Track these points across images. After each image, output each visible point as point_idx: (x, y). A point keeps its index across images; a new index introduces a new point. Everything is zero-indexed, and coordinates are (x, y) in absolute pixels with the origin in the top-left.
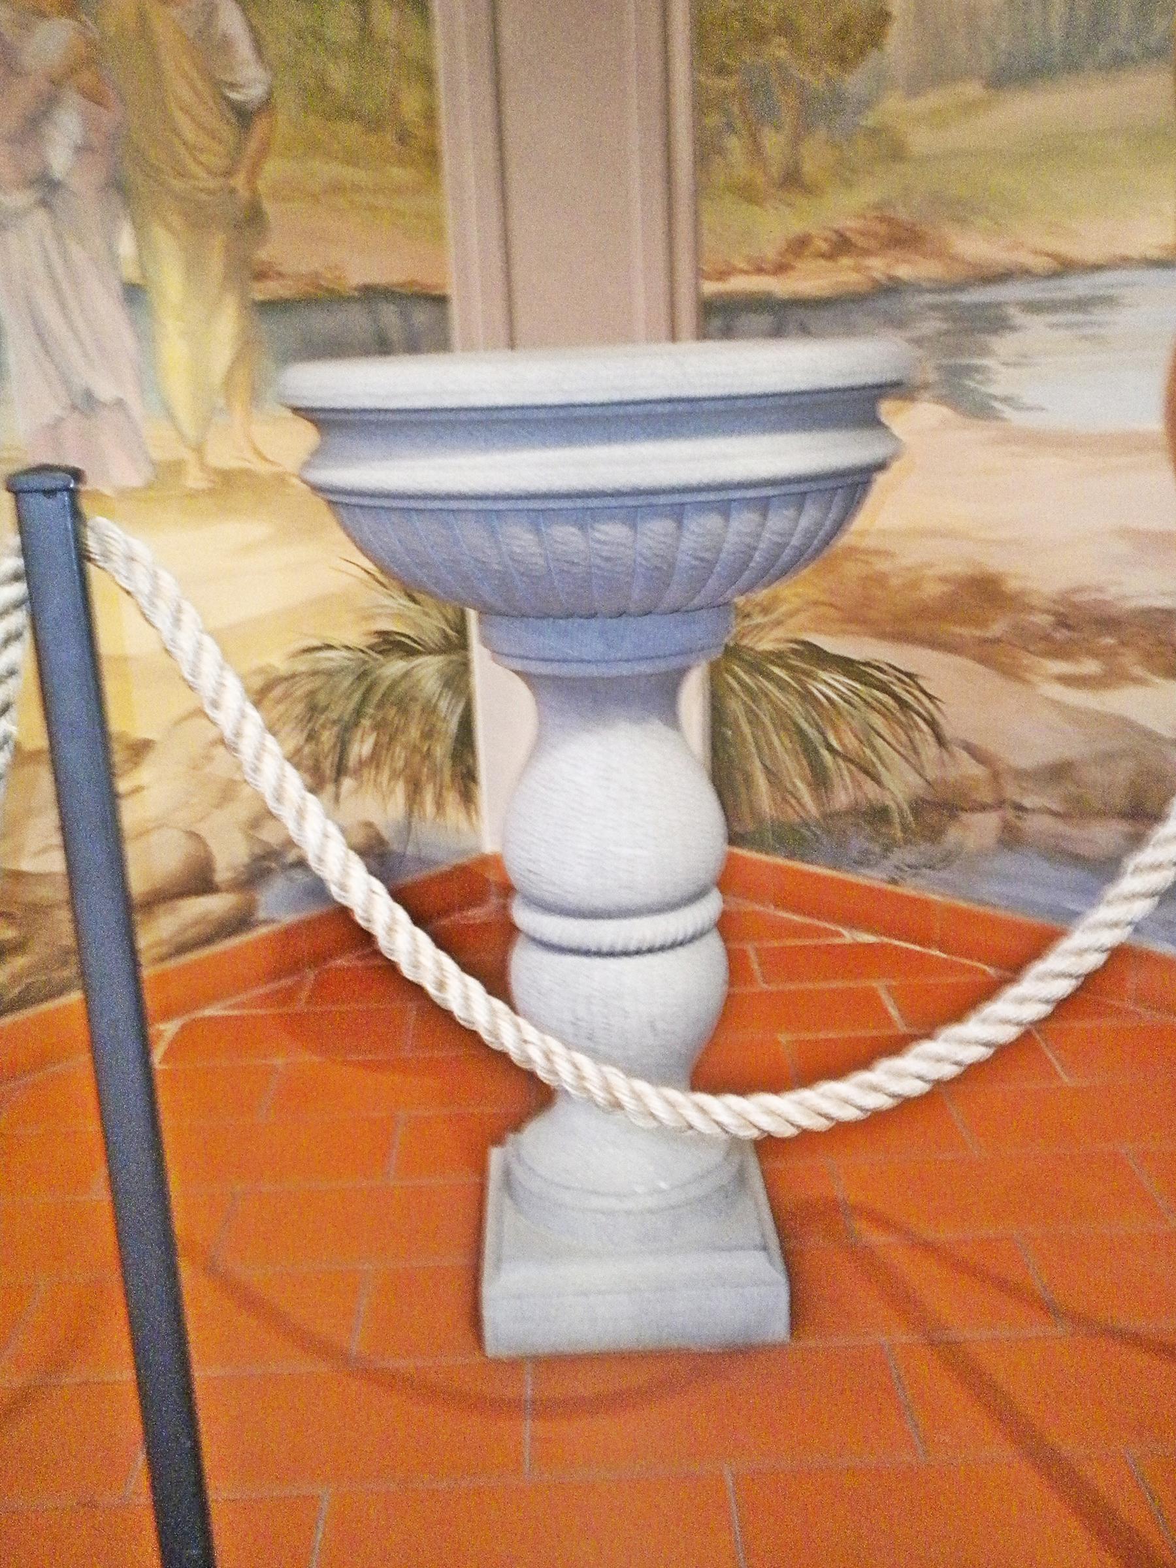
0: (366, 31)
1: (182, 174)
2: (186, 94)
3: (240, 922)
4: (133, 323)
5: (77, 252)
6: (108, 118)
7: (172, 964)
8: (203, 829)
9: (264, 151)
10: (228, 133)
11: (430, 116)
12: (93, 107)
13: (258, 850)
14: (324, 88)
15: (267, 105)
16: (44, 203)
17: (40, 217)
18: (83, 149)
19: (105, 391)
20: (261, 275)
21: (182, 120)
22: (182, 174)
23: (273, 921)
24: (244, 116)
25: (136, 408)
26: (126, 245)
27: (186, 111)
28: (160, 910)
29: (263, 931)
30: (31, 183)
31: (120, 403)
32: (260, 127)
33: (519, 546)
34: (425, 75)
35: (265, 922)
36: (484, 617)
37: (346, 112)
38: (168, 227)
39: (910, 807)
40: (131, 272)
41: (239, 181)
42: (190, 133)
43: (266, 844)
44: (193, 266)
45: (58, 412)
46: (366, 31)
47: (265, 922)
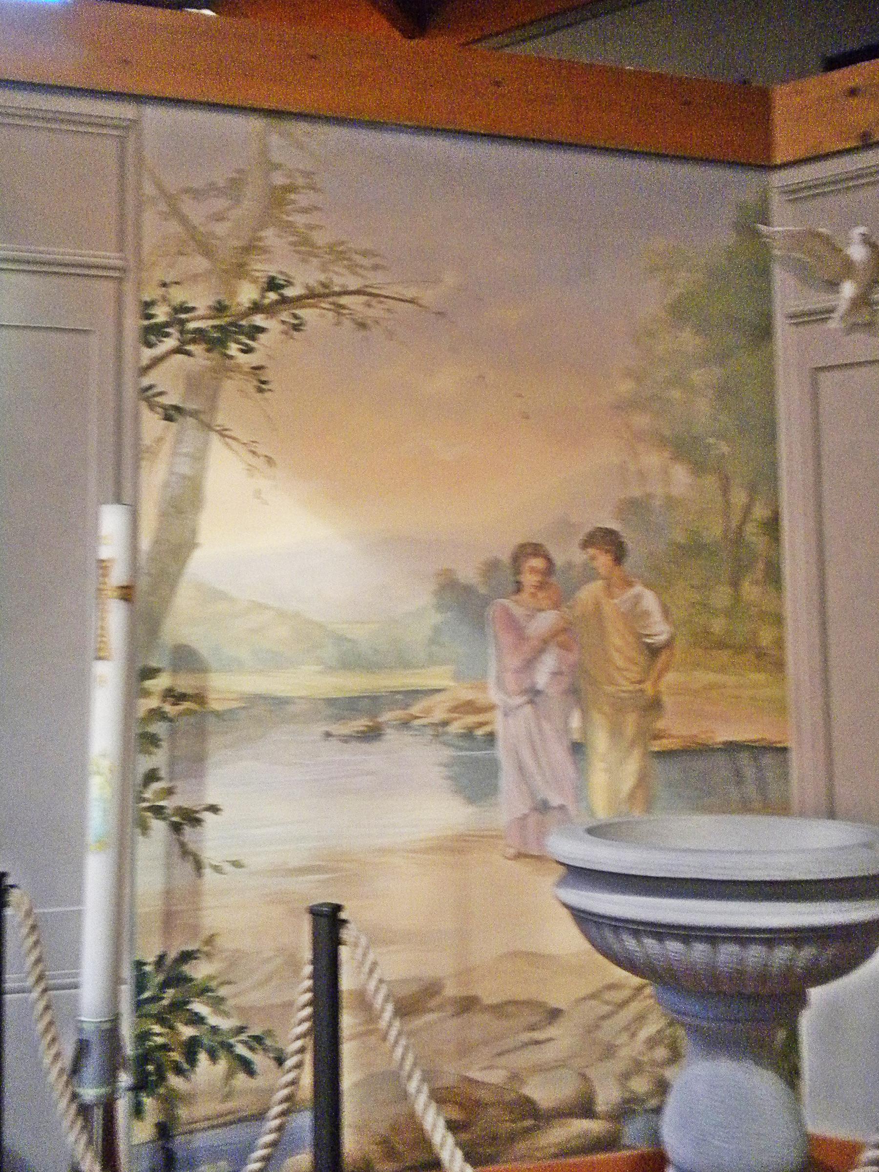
0: (737, 598)
1: (612, 683)
2: (617, 641)
3: (609, 1143)
4: (575, 763)
5: (546, 726)
6: (572, 657)
7: (563, 1161)
8: (591, 1073)
9: (666, 669)
10: (642, 659)
11: (779, 643)
12: (564, 652)
13: (627, 1095)
14: (707, 632)
15: (668, 645)
16: (531, 702)
17: (528, 709)
18: (556, 674)
19: (555, 800)
20: (657, 737)
21: (616, 656)
22: (612, 683)
23: (634, 1148)
24: (654, 651)
25: (572, 808)
26: (575, 721)
27: (617, 650)
28: (555, 1122)
29: (626, 1153)
30: (525, 692)
31: (562, 808)
32: (663, 657)
33: (261, 984)
34: (778, 620)
35: (629, 1147)
36: (421, 1157)
37: (721, 645)
38: (600, 711)
39: (117, 252)
40: (576, 736)
41: (648, 687)
42: (620, 663)
43: (632, 1092)
44: (616, 732)
45: (526, 811)
46: (737, 598)
47: (629, 1147)
